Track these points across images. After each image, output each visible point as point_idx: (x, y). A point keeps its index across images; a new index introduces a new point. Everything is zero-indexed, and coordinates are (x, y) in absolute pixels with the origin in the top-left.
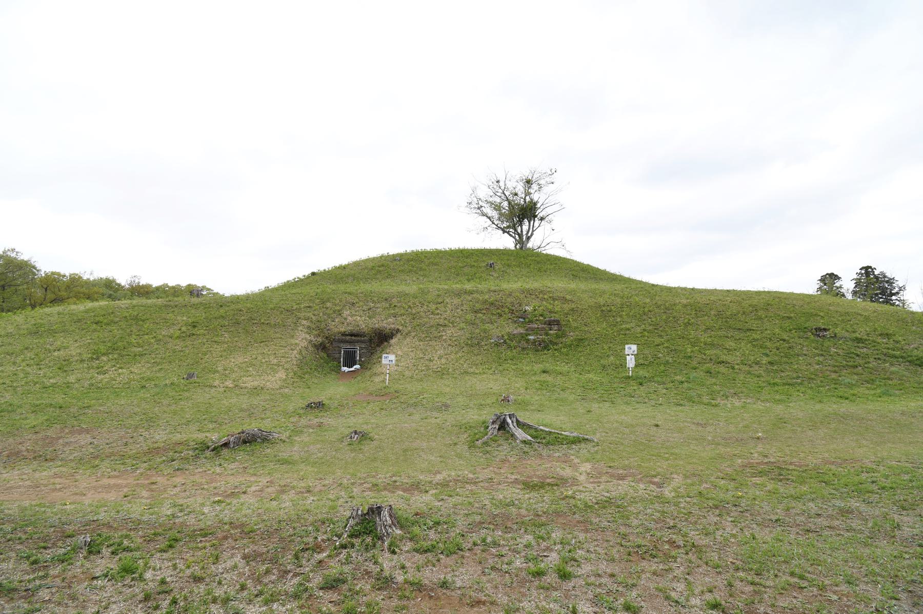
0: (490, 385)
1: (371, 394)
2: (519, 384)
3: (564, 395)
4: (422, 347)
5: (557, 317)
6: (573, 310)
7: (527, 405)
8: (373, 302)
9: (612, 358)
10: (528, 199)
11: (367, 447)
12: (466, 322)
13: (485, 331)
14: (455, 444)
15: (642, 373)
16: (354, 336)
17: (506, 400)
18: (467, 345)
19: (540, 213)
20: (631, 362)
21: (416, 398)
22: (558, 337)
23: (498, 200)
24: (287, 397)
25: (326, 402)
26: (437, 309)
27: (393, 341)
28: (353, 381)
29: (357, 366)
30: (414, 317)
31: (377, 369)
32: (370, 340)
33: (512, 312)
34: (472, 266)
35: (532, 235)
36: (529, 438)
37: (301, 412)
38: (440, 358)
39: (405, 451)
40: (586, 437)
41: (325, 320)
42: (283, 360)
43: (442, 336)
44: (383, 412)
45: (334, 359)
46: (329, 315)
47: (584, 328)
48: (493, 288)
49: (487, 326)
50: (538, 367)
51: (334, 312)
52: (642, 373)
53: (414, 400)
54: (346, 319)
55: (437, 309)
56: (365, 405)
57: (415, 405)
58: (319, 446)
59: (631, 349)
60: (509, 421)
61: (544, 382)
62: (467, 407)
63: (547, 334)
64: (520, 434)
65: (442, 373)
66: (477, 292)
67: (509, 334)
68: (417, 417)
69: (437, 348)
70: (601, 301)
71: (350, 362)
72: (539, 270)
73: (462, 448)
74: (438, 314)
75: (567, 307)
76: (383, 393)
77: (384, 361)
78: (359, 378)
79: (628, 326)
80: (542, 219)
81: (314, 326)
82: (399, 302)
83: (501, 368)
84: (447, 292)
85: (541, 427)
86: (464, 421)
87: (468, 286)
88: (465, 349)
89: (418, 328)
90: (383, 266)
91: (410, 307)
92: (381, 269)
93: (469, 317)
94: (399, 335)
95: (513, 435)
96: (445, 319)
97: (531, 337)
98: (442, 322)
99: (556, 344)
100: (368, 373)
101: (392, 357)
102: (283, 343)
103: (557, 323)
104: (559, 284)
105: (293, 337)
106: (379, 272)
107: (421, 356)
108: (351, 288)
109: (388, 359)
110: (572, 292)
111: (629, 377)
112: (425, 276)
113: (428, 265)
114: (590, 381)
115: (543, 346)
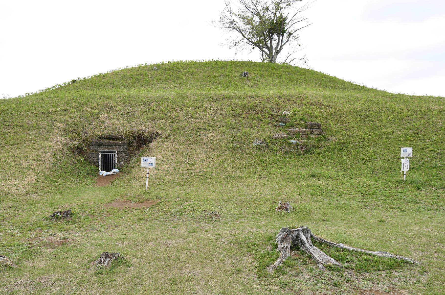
0: (259, 190)
1: (129, 201)
2: (290, 189)
3: (345, 201)
4: (182, 150)
5: (318, 121)
6: (331, 115)
7: (309, 214)
8: (132, 106)
9: (379, 162)
10: (278, 15)
11: (122, 277)
12: (226, 125)
13: (246, 135)
14: (239, 271)
15: (415, 177)
16: (112, 139)
17: (283, 207)
18: (229, 148)
19: (289, 28)
20: (405, 165)
21: (180, 205)
22: (320, 140)
23: (250, 15)
24: (32, 204)
25: (75, 210)
26: (196, 113)
27: (152, 145)
28: (110, 185)
29: (116, 170)
30: (173, 120)
31: (135, 173)
32: (129, 144)
33: (271, 116)
34: (227, 76)
35: (281, 49)
36: (333, 261)
37: (45, 223)
38: (202, 161)
39: (173, 283)
40: (405, 259)
41: (82, 123)
42: (35, 163)
43: (202, 139)
44: (143, 223)
45: (92, 163)
46: (86, 118)
47: (345, 132)
48: (250, 94)
49: (248, 130)
50: (305, 171)
51: (92, 115)
52: (415, 177)
53: (178, 208)
54: (103, 122)
55: (196, 113)
56: (121, 214)
57: (180, 214)
58: (55, 276)
59: (407, 152)
60: (303, 238)
61: (317, 187)
62: (239, 216)
63: (308, 138)
64: (318, 253)
65: (205, 177)
66: (235, 97)
67: (270, 138)
68: (183, 230)
69: (198, 151)
70: (358, 106)
71: (108, 165)
72: (290, 80)
73: (249, 278)
74: (197, 118)
75: (326, 112)
76: (143, 200)
77: (143, 164)
78: (117, 182)
79: (389, 130)
80: (290, 34)
81: (70, 129)
82: (157, 106)
83: (266, 172)
84: (205, 97)
85: (341, 245)
86: (242, 237)
87: (226, 93)
88: (227, 152)
89: (177, 131)
90: (141, 74)
91: (169, 111)
92: (140, 77)
93: (229, 121)
94: (158, 139)
95: (311, 257)
96: (205, 123)
97: (293, 141)
98: (202, 125)
99: (318, 148)
100: (127, 177)
101: (152, 160)
102: (36, 145)
103: (318, 126)
104: (313, 92)
105: (47, 139)
106: (138, 80)
107: (183, 159)
108: (109, 92)
109: (148, 161)
110: (328, 98)
111: (402, 182)
112: (182, 84)
113: (185, 75)
114: (364, 185)
115: (305, 150)
